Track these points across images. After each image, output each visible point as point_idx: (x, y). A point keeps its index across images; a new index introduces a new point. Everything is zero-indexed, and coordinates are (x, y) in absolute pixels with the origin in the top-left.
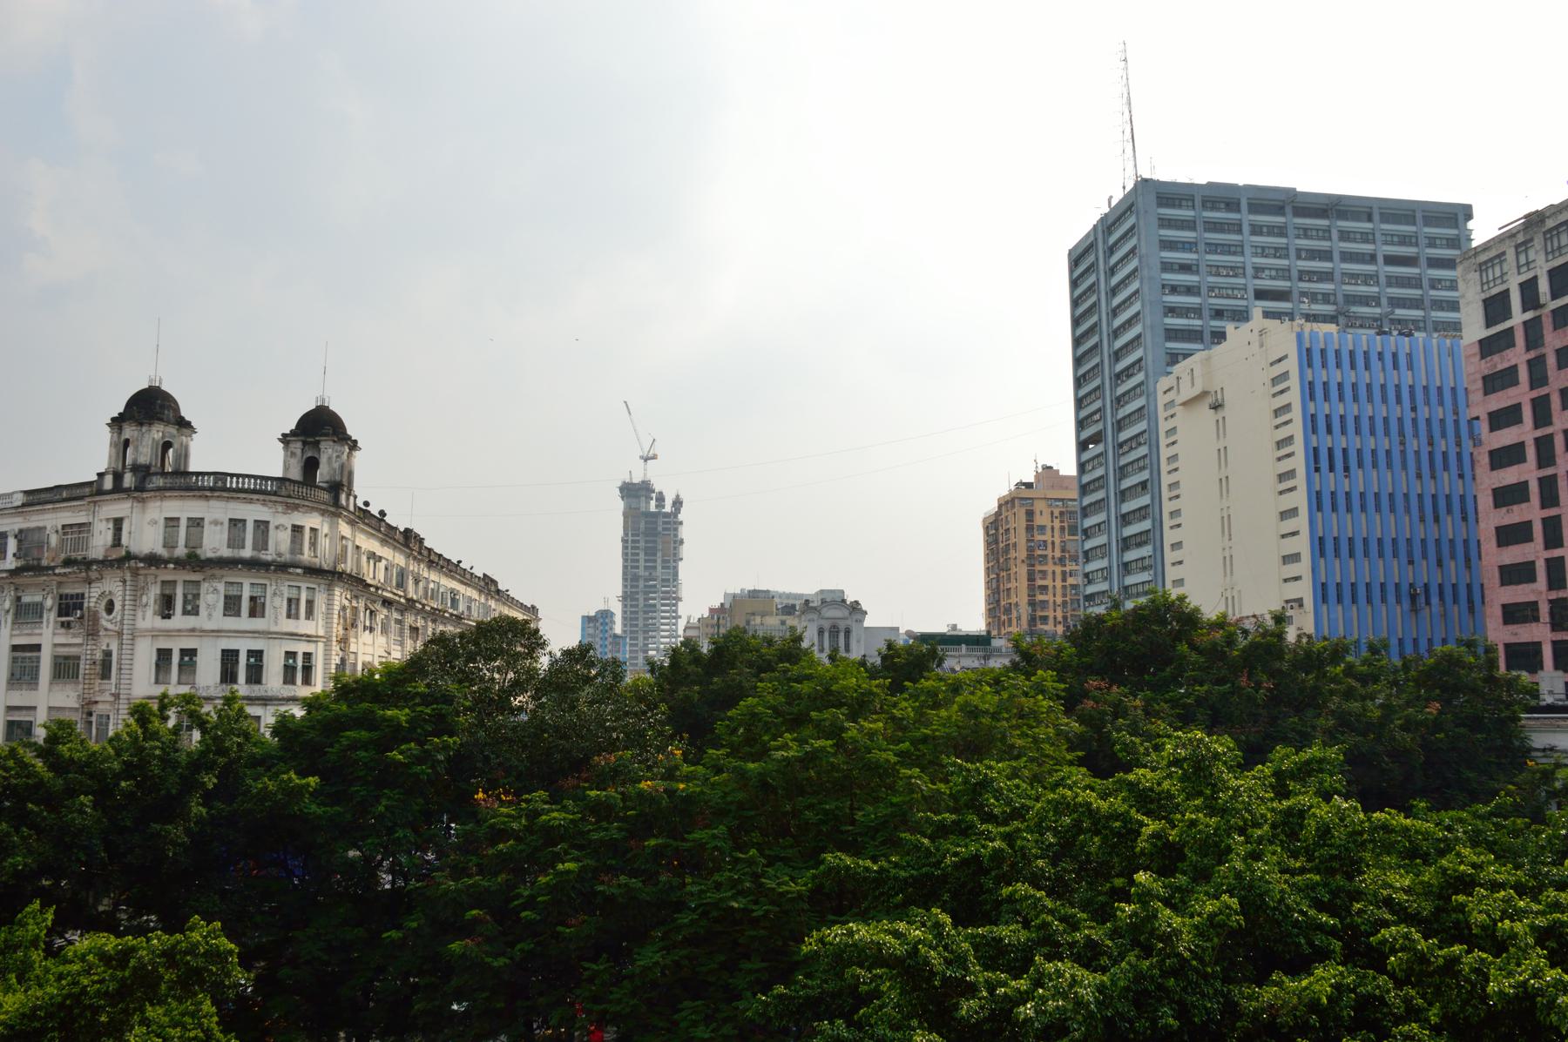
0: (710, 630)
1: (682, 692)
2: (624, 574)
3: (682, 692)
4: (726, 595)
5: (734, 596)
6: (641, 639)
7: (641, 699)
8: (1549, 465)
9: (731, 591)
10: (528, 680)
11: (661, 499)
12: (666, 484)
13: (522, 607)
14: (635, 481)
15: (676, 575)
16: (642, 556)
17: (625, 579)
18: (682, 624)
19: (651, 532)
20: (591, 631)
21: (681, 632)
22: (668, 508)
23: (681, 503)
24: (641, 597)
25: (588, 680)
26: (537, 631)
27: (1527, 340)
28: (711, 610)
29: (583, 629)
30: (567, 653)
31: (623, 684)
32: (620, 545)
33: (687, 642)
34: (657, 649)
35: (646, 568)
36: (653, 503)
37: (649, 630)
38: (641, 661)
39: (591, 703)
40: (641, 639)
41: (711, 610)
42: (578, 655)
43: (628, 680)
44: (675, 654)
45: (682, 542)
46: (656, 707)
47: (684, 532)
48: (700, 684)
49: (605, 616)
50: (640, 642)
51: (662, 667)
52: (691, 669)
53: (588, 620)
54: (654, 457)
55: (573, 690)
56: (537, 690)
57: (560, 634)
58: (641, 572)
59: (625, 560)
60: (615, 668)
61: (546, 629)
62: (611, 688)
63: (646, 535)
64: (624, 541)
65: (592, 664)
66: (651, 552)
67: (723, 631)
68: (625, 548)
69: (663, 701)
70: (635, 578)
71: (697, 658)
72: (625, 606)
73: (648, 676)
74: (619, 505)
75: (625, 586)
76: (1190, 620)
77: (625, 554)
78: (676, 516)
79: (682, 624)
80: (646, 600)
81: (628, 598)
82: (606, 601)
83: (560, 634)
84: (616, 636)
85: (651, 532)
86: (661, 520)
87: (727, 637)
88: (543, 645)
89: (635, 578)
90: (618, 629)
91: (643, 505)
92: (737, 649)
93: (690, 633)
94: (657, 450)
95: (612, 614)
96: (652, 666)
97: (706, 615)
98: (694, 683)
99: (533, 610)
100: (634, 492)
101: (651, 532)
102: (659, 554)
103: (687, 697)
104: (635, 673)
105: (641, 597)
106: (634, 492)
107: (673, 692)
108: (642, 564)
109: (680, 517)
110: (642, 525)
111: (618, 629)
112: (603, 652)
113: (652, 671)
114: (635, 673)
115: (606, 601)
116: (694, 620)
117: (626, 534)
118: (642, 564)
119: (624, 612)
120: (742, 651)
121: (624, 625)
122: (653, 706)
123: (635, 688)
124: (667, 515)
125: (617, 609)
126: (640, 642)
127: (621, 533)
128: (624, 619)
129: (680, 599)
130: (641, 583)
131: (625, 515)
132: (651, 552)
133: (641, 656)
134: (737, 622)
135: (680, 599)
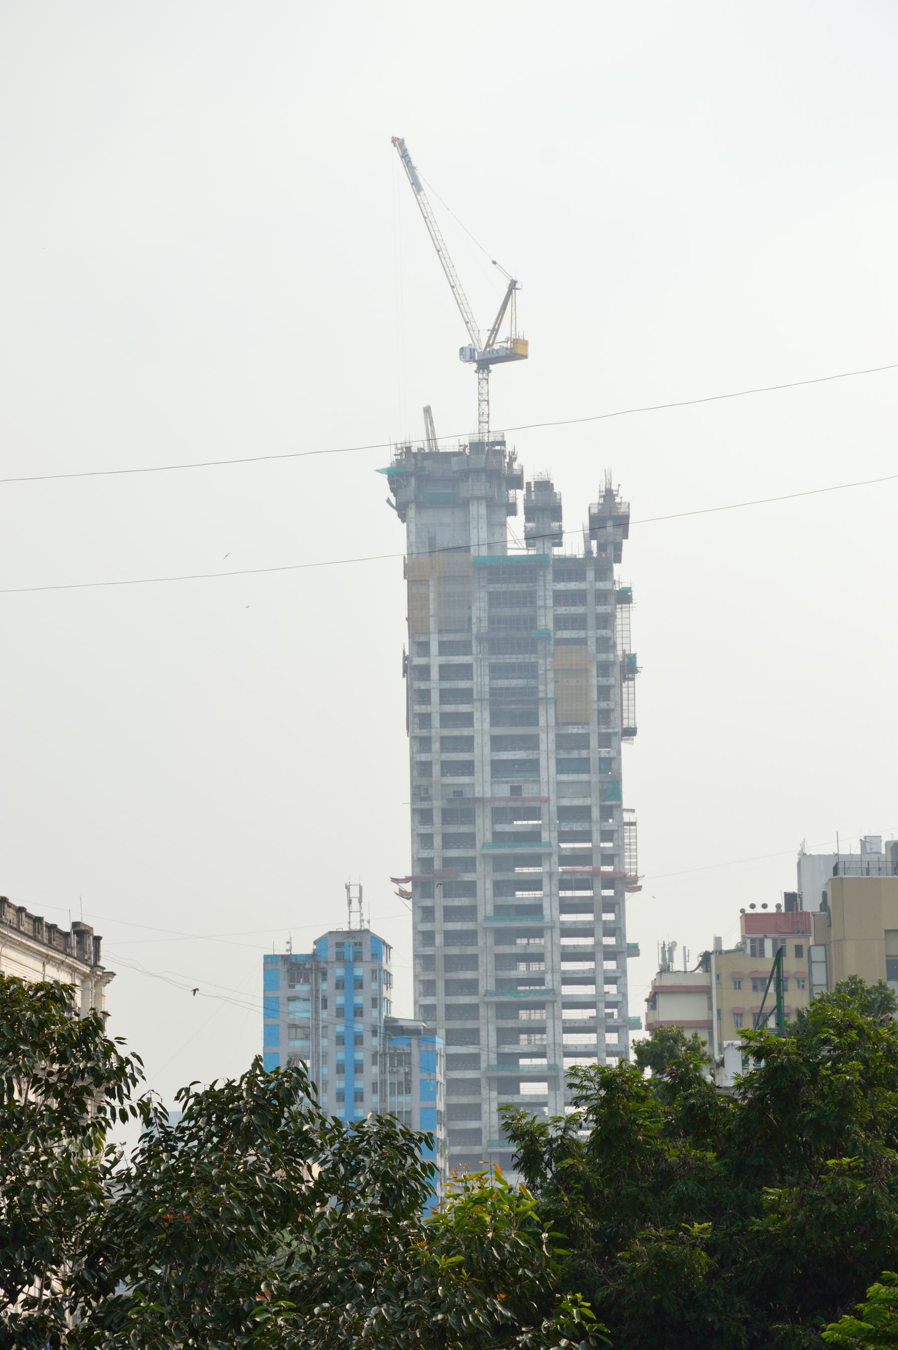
0: (750, 1000)
1: (646, 1244)
2: (419, 793)
3: (646, 1244)
4: (804, 862)
5: (838, 866)
6: (489, 1037)
7: (490, 1276)
8: (605, 628)
9: (823, 846)
10: (62, 1221)
11: (545, 507)
12: (562, 448)
13: (41, 932)
14: (448, 444)
15: (611, 790)
16: (482, 727)
17: (421, 815)
18: (641, 976)
19: (514, 636)
20: (301, 1012)
21: (637, 1008)
22: (574, 543)
23: (622, 523)
24: (484, 879)
25: (289, 1207)
26: (94, 1025)
27: (449, 737)
28: (752, 922)
29: (270, 1008)
30: (212, 1105)
31: (424, 1218)
32: (396, 690)
33: (662, 1049)
34: (548, 1077)
35: (498, 767)
36: (516, 526)
37: (520, 1001)
38: (490, 1121)
39: (302, 1298)
40: (489, 1037)
41: (752, 922)
42: (252, 1113)
43: (444, 1198)
44: (613, 1093)
45: (629, 668)
46: (550, 1307)
47: (639, 631)
48: (713, 1212)
49: (351, 953)
50: (488, 1046)
51: (566, 1148)
52: (674, 1152)
53: (288, 972)
54: (515, 352)
55: (232, 1249)
56: (94, 1252)
57: (183, 1032)
58: (482, 785)
59: (421, 743)
60: (390, 1157)
61: (130, 1018)
62: (374, 1239)
63: (494, 646)
64: (414, 671)
65: (302, 1146)
66: (515, 710)
67: (797, 1000)
68: (417, 697)
69: (574, 1280)
70: (461, 809)
71: (698, 1114)
72: (425, 914)
73: (516, 1180)
74: (392, 538)
75: (422, 840)
76: (392, 468)
77: (418, 722)
78: (604, 572)
79: (641, 976)
80: (501, 888)
81: (431, 883)
82: (354, 896)
83: (183, 1032)
84: (394, 1029)
85: (514, 624)
86: (548, 588)
87: (811, 1026)
88: (117, 1076)
89: (461, 809)
90: (402, 1003)
91: (479, 534)
92: (852, 1072)
93: (675, 1011)
94: (525, 322)
95: (379, 947)
96: (531, 1147)
97: (732, 939)
98: (689, 1208)
99: (80, 942)
100: (441, 485)
101: (514, 624)
102: (546, 716)
103: (662, 1261)
104: (467, 1174)
105: (484, 879)
106: (441, 485)
107: (611, 1243)
108: (483, 753)
109: (623, 574)
110: (479, 611)
111: (402, 1003)
112: (341, 1098)
113: (529, 1163)
114: (467, 1174)
115: (354, 896)
116: (686, 962)
117: (419, 645)
118: (483, 753)
119: (424, 938)
120: (870, 1081)
121: (425, 987)
122: (536, 1305)
123: (467, 1233)
124: (569, 569)
125: (394, 923)
126: (488, 1046)
127: (399, 639)
128: (423, 961)
129: (631, 884)
130: (483, 827)
131: (415, 575)
132: (515, 710)
133: (491, 1102)
134: (851, 969)
135: (631, 884)
